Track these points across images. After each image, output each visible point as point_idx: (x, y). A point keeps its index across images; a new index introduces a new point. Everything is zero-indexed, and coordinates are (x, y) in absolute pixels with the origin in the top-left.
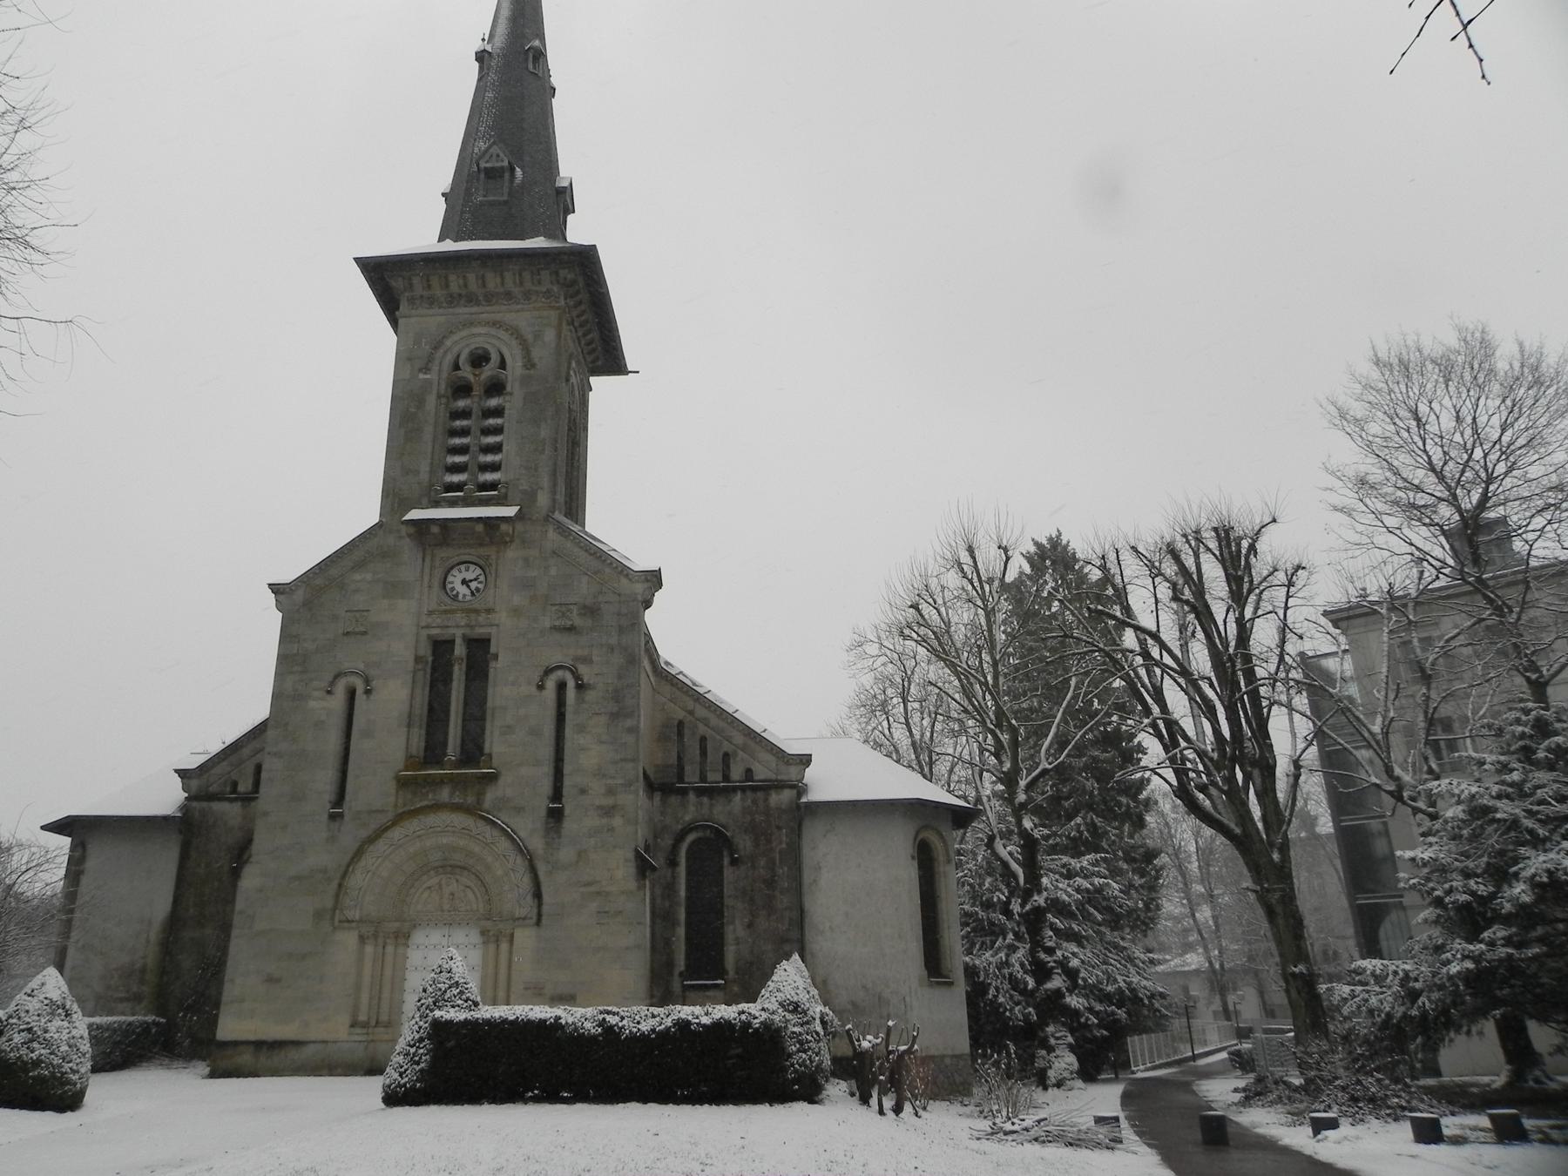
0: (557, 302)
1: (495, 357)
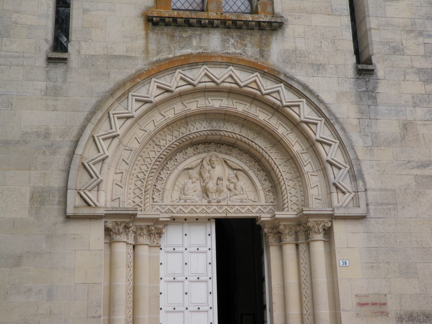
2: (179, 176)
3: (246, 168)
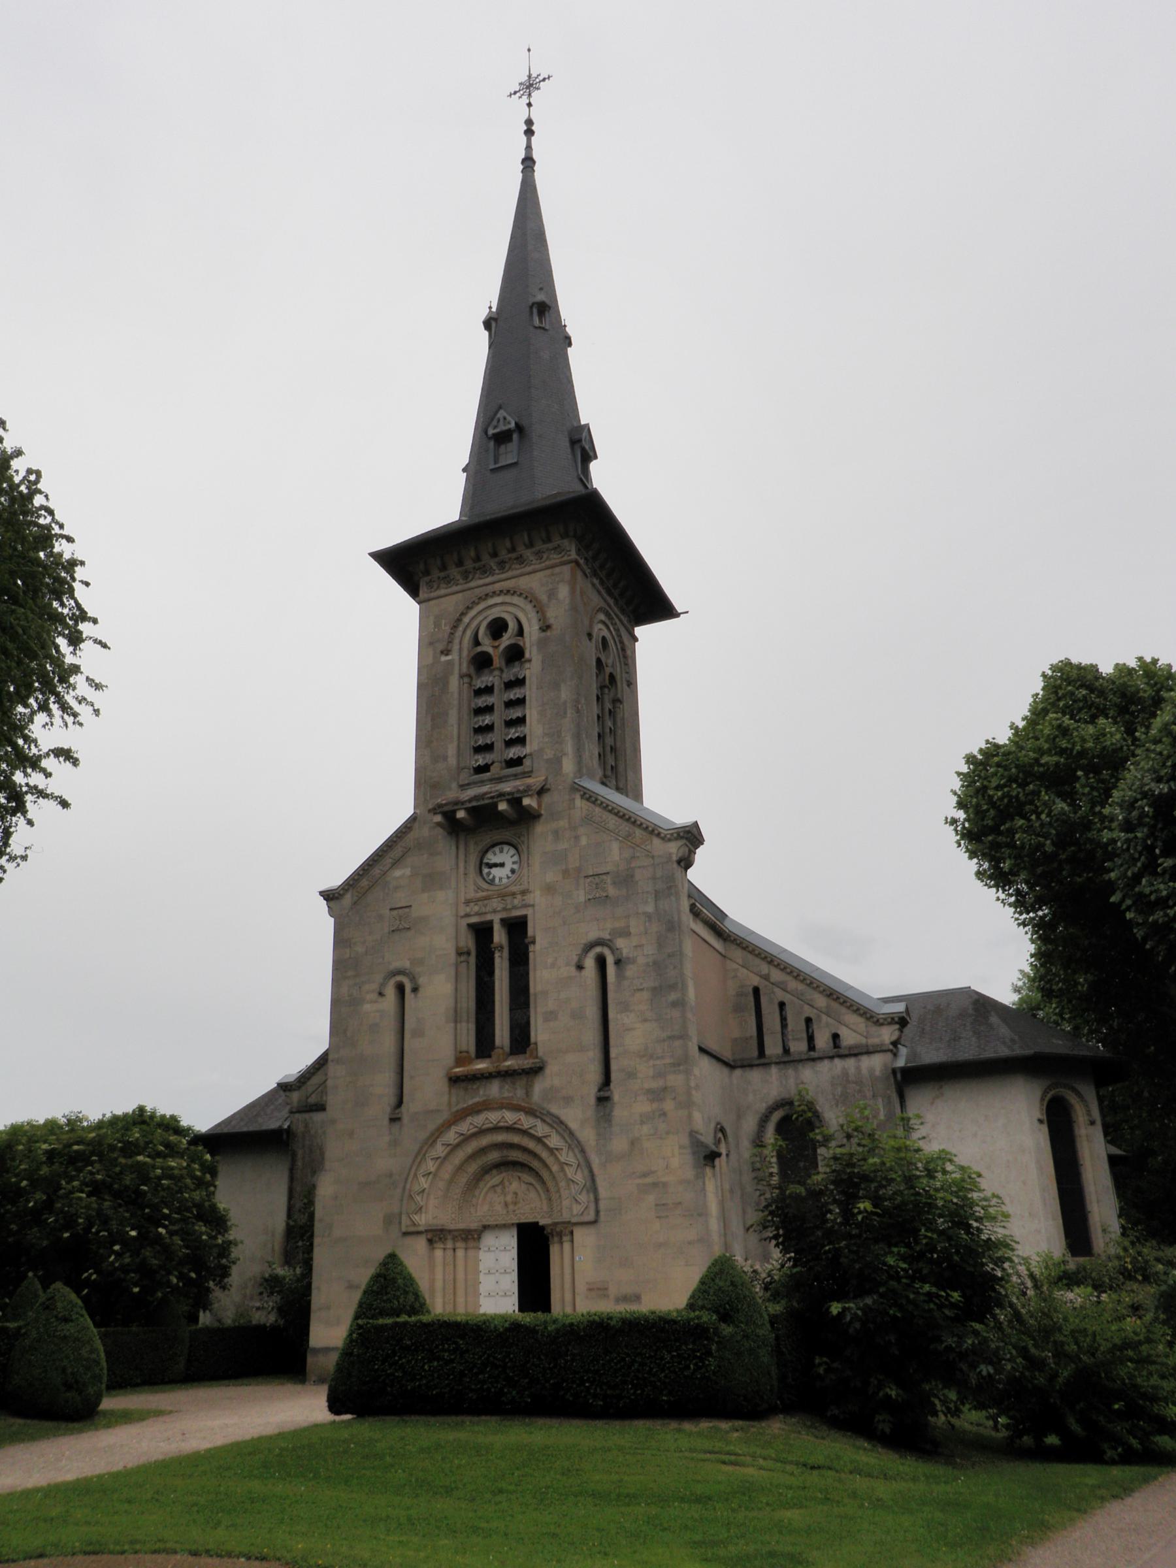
1: (512, 625)
3: (534, 1183)
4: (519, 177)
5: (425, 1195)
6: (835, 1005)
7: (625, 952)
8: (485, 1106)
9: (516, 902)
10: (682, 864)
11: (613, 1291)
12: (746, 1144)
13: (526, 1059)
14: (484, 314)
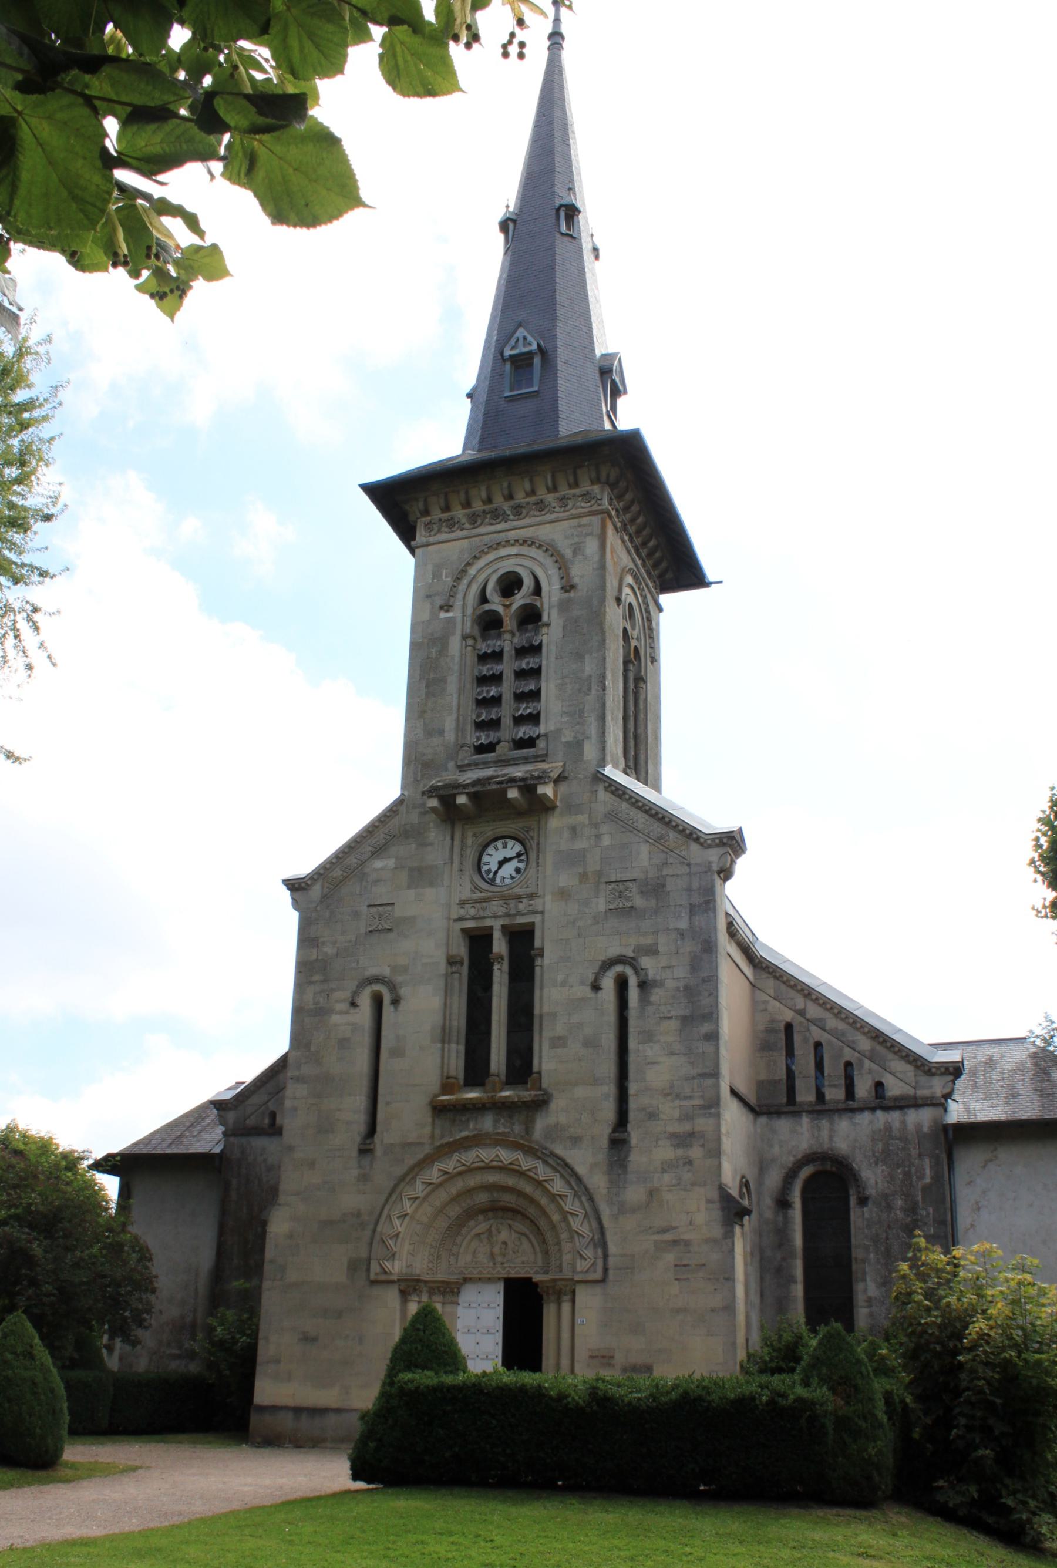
0: (599, 505)
1: (528, 583)
2: (471, 1240)
4: (545, 54)
5: (400, 1240)
6: (879, 1048)
7: (651, 974)
8: (477, 1141)
9: (521, 907)
10: (722, 875)
11: (619, 1359)
12: (768, 1201)
13: (527, 1090)
14: (500, 215)
